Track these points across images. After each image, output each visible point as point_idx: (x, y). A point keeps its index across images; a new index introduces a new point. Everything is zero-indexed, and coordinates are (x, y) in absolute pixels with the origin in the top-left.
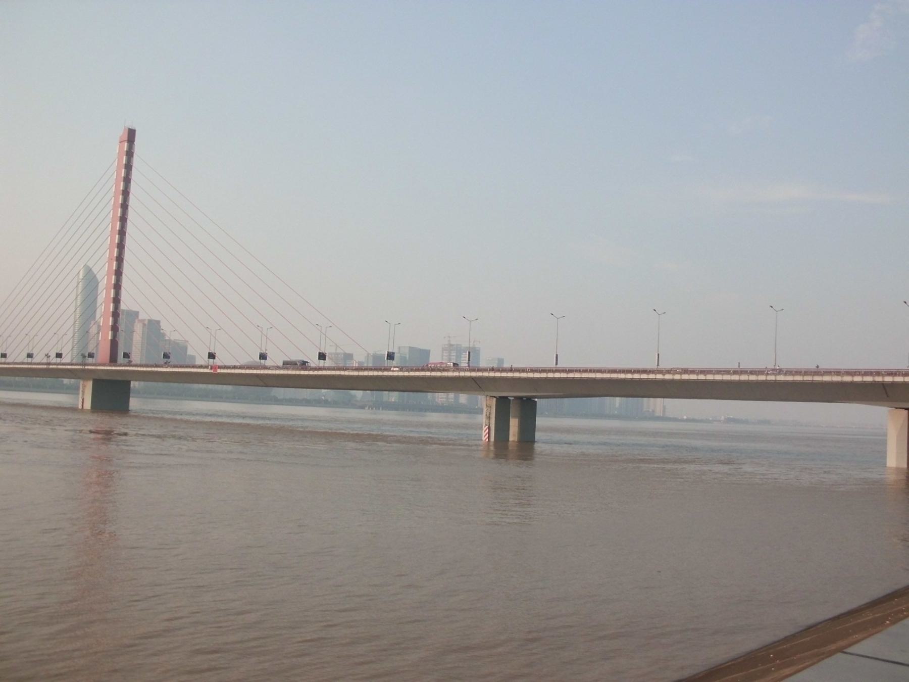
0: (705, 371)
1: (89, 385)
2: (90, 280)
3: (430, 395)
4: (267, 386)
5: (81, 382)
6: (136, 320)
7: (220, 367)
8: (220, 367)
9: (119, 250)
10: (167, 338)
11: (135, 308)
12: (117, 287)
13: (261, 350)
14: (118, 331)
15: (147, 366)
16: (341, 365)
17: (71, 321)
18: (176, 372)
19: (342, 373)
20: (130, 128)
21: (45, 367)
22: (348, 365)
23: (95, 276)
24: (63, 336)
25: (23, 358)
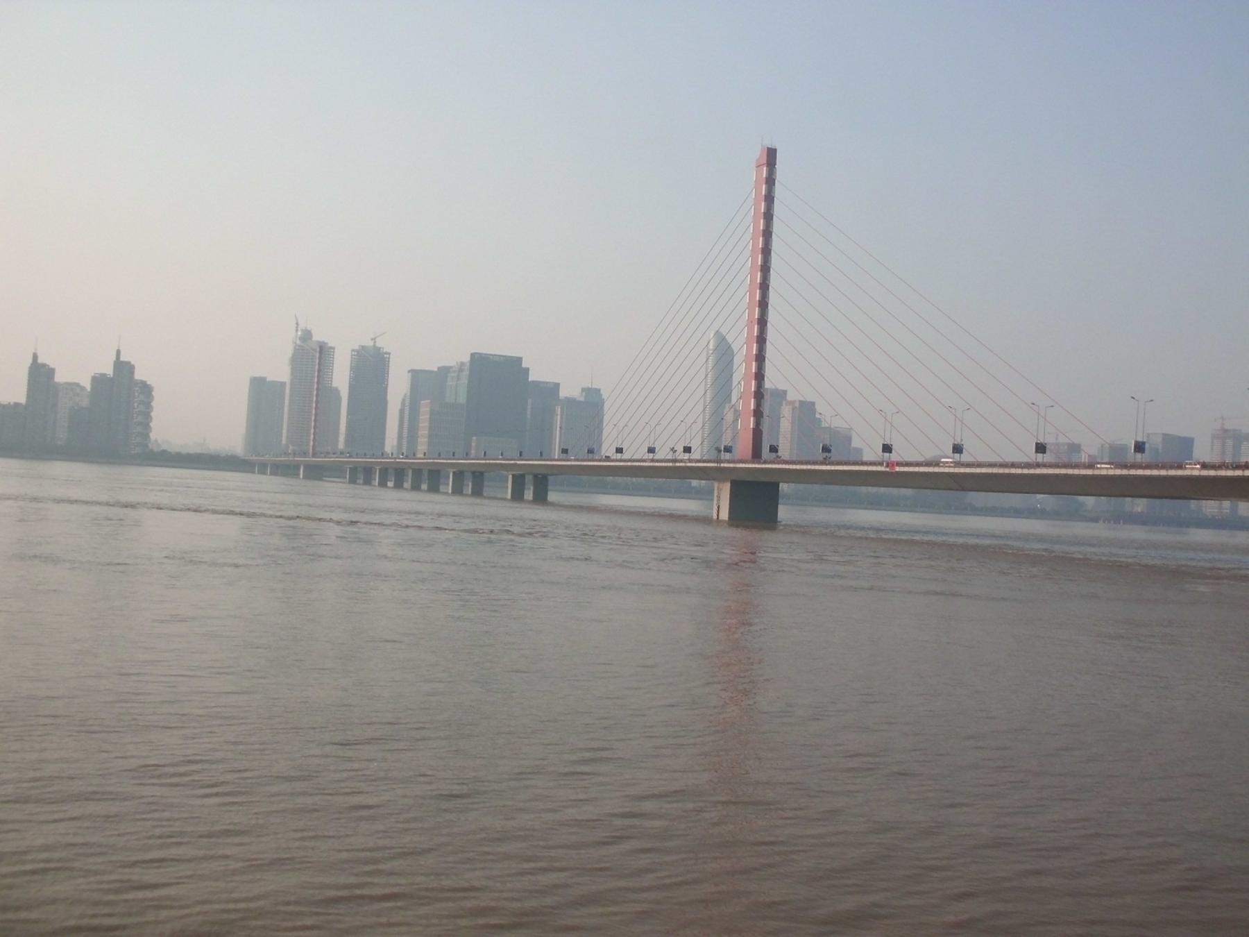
1: (726, 488)
2: (723, 352)
3: (1193, 504)
4: (963, 490)
5: (716, 484)
6: (784, 402)
7: (899, 464)
8: (899, 464)
9: (762, 310)
10: (826, 425)
11: (781, 387)
12: (760, 358)
13: (955, 440)
14: (762, 417)
15: (801, 463)
16: (1065, 459)
17: (700, 407)
18: (856, 471)
19: (1070, 471)
20: (770, 147)
21: (671, 464)
22: (1075, 459)
23: (730, 346)
24: (624, 428)
25: (642, 453)
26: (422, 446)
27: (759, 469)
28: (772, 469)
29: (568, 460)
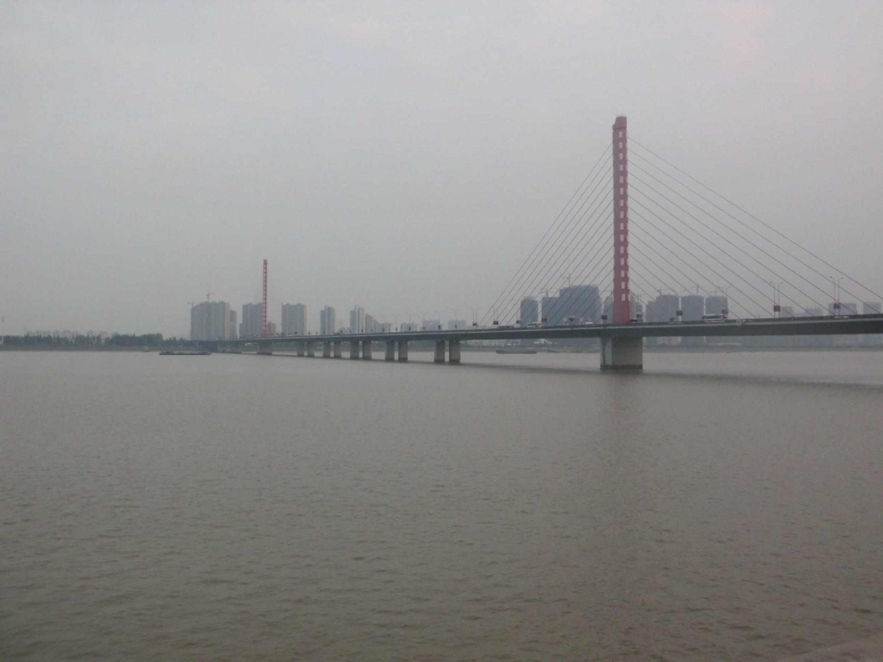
24: (498, 308)
25: (315, 334)
26: (238, 333)
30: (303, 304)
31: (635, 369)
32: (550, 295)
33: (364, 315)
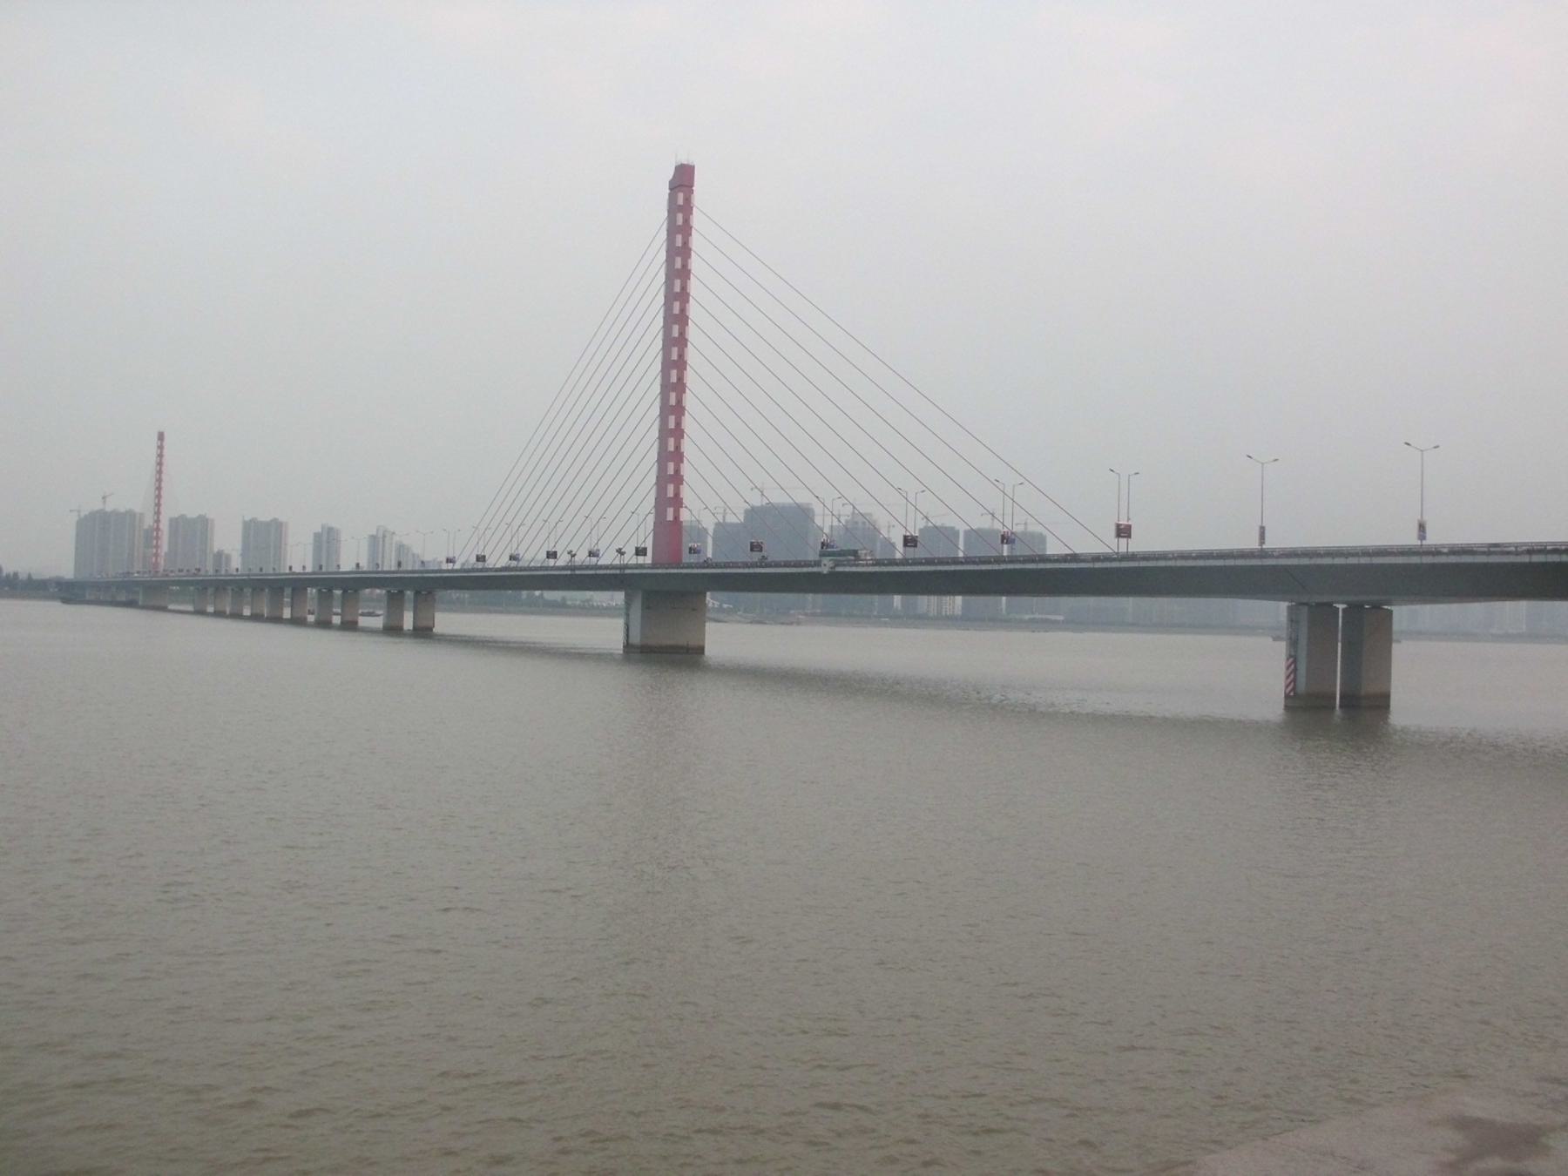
0: (1332, 554)
25: (504, 561)
27: (974, 572)
28: (964, 571)
29: (857, 565)
30: (207, 516)
31: (687, 657)
32: (731, 519)
33: (394, 545)
